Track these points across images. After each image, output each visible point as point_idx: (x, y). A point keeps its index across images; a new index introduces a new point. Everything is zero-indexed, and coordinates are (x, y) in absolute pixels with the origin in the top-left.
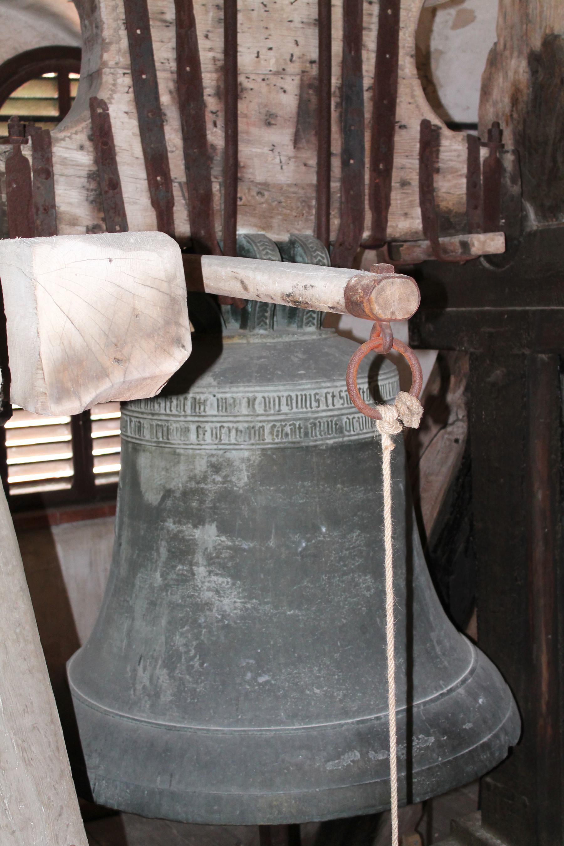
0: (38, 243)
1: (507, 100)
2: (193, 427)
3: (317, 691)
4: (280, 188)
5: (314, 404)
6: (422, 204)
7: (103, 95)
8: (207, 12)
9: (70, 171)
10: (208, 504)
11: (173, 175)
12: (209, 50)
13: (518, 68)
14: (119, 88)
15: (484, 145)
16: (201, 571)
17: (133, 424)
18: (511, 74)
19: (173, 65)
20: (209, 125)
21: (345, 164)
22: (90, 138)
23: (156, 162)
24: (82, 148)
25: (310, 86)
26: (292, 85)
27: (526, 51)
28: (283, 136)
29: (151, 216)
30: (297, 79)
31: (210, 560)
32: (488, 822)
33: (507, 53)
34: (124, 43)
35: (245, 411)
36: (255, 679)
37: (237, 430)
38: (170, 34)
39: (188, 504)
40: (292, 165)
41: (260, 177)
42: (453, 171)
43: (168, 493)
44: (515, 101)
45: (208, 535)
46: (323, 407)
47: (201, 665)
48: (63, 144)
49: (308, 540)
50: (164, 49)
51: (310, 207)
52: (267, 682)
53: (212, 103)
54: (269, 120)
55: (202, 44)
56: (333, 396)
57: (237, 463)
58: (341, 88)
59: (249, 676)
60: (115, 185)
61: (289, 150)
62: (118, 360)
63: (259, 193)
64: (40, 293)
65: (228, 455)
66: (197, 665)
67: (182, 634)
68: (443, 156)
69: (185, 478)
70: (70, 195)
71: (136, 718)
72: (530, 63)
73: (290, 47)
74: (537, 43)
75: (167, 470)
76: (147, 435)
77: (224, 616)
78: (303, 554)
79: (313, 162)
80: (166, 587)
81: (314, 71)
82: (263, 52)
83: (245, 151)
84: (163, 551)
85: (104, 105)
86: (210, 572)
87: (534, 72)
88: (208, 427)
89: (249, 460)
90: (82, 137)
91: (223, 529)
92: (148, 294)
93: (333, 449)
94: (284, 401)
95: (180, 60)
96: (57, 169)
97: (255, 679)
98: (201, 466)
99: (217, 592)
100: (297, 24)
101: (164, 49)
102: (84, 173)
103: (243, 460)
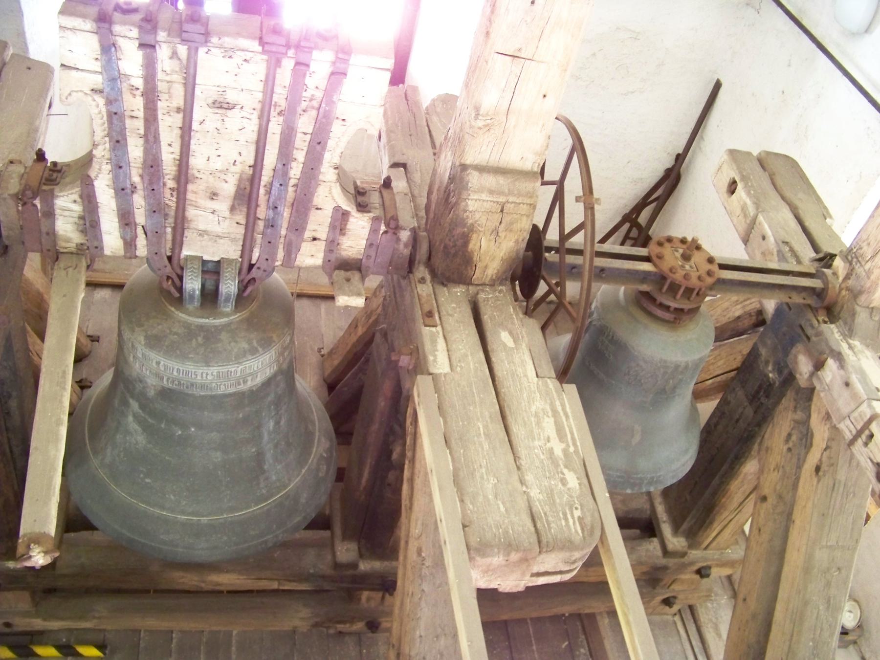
3: (172, 497)
14: (103, 171)
24: (75, 201)
28: (223, 206)
41: (202, 227)
50: (135, 150)
56: (207, 374)
61: (227, 214)
71: (435, 305)
73: (235, 156)
94: (175, 370)
96: (58, 212)
101: (135, 150)
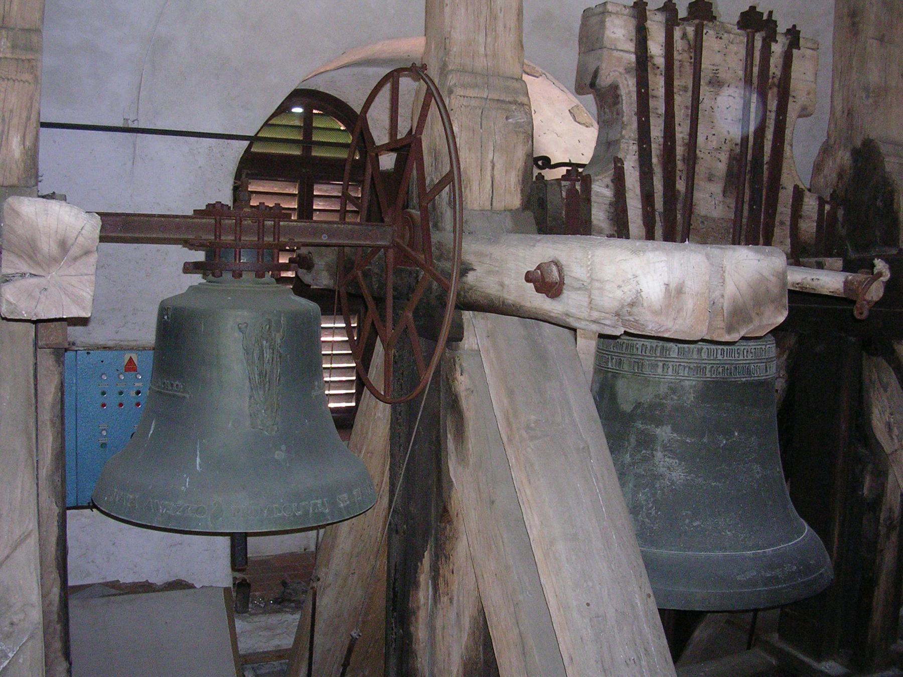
0: (539, 241)
1: (834, 175)
2: (661, 364)
4: (714, 220)
5: (737, 355)
6: (791, 236)
7: (620, 156)
8: (681, 110)
9: (601, 200)
10: (667, 413)
11: (657, 206)
12: (681, 132)
13: (843, 157)
15: (827, 203)
16: (659, 455)
17: (614, 361)
18: (838, 160)
19: (661, 140)
20: (678, 178)
21: (751, 206)
22: (612, 181)
23: (647, 198)
24: (607, 186)
25: (735, 159)
26: (724, 157)
27: (850, 147)
28: (717, 188)
29: (643, 232)
30: (727, 156)
31: (665, 448)
32: (782, 637)
33: (836, 146)
34: (635, 125)
35: (695, 356)
36: (691, 523)
37: (689, 368)
38: (661, 121)
39: (652, 413)
40: (721, 207)
41: (703, 213)
42: (810, 218)
43: (639, 405)
44: (840, 176)
45: (664, 433)
46: (741, 358)
47: (656, 513)
48: (597, 183)
49: (727, 440)
50: (657, 131)
51: (729, 233)
52: (698, 526)
53: (680, 165)
54: (710, 179)
55: (678, 129)
57: (687, 388)
58: (751, 162)
59: (687, 521)
60: (625, 210)
62: (757, 314)
63: (702, 222)
64: (726, 275)
65: (682, 383)
66: (653, 513)
67: (643, 494)
68: (805, 207)
69: (652, 396)
70: (599, 215)
72: (852, 154)
74: (858, 143)
75: (639, 390)
76: (626, 367)
77: (673, 483)
78: (724, 448)
79: (733, 205)
80: (633, 464)
81: (738, 150)
82: (710, 136)
83: (697, 195)
84: (633, 440)
85: (621, 161)
86: (665, 456)
87: (855, 161)
88: (670, 364)
89: (695, 386)
90: (608, 180)
91: (675, 429)
92: (773, 279)
93: (744, 384)
95: (665, 137)
96: (593, 198)
97: (691, 523)
98: (663, 389)
99: (669, 468)
100: (729, 120)
101: (657, 131)
102: (608, 202)
103: (691, 387)
